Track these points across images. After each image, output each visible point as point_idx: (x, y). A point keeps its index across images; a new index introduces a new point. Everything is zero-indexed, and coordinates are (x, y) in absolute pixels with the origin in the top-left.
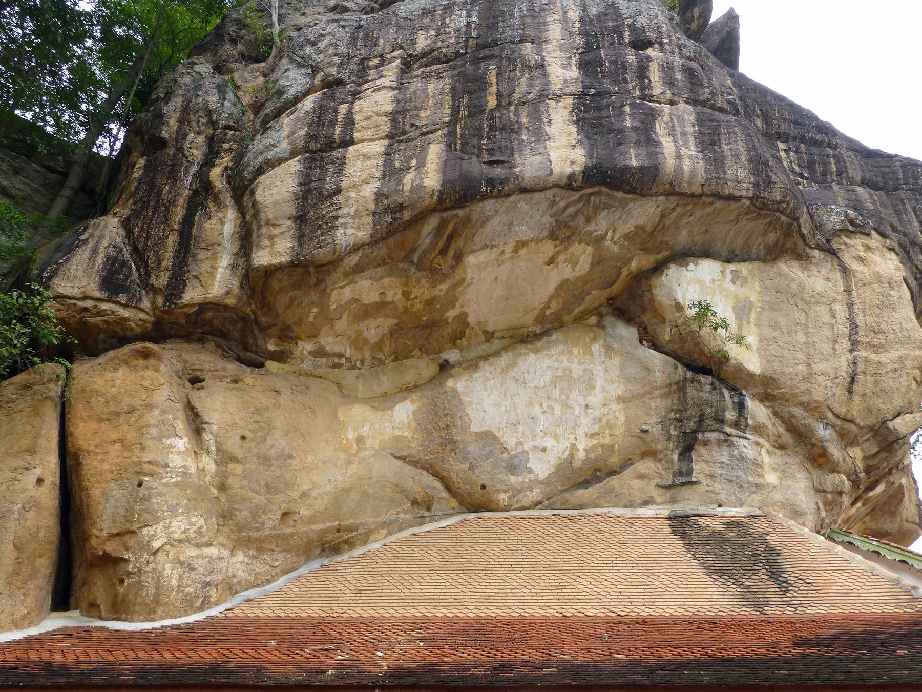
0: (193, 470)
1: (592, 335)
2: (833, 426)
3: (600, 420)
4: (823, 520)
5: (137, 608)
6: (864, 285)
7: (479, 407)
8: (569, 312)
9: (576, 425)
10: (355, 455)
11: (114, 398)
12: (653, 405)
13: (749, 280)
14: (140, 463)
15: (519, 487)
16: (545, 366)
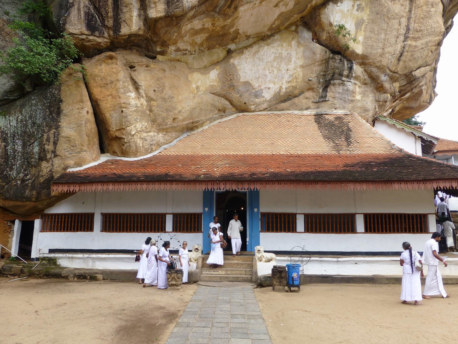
0: (139, 105)
1: (292, 36)
2: (388, 75)
3: (292, 75)
4: (377, 112)
5: (131, 154)
6: (419, 7)
7: (244, 71)
8: (283, 25)
9: (283, 78)
10: (196, 94)
11: (104, 78)
12: (315, 69)
13: (365, 9)
14: (120, 104)
15: (259, 103)
16: (271, 52)
